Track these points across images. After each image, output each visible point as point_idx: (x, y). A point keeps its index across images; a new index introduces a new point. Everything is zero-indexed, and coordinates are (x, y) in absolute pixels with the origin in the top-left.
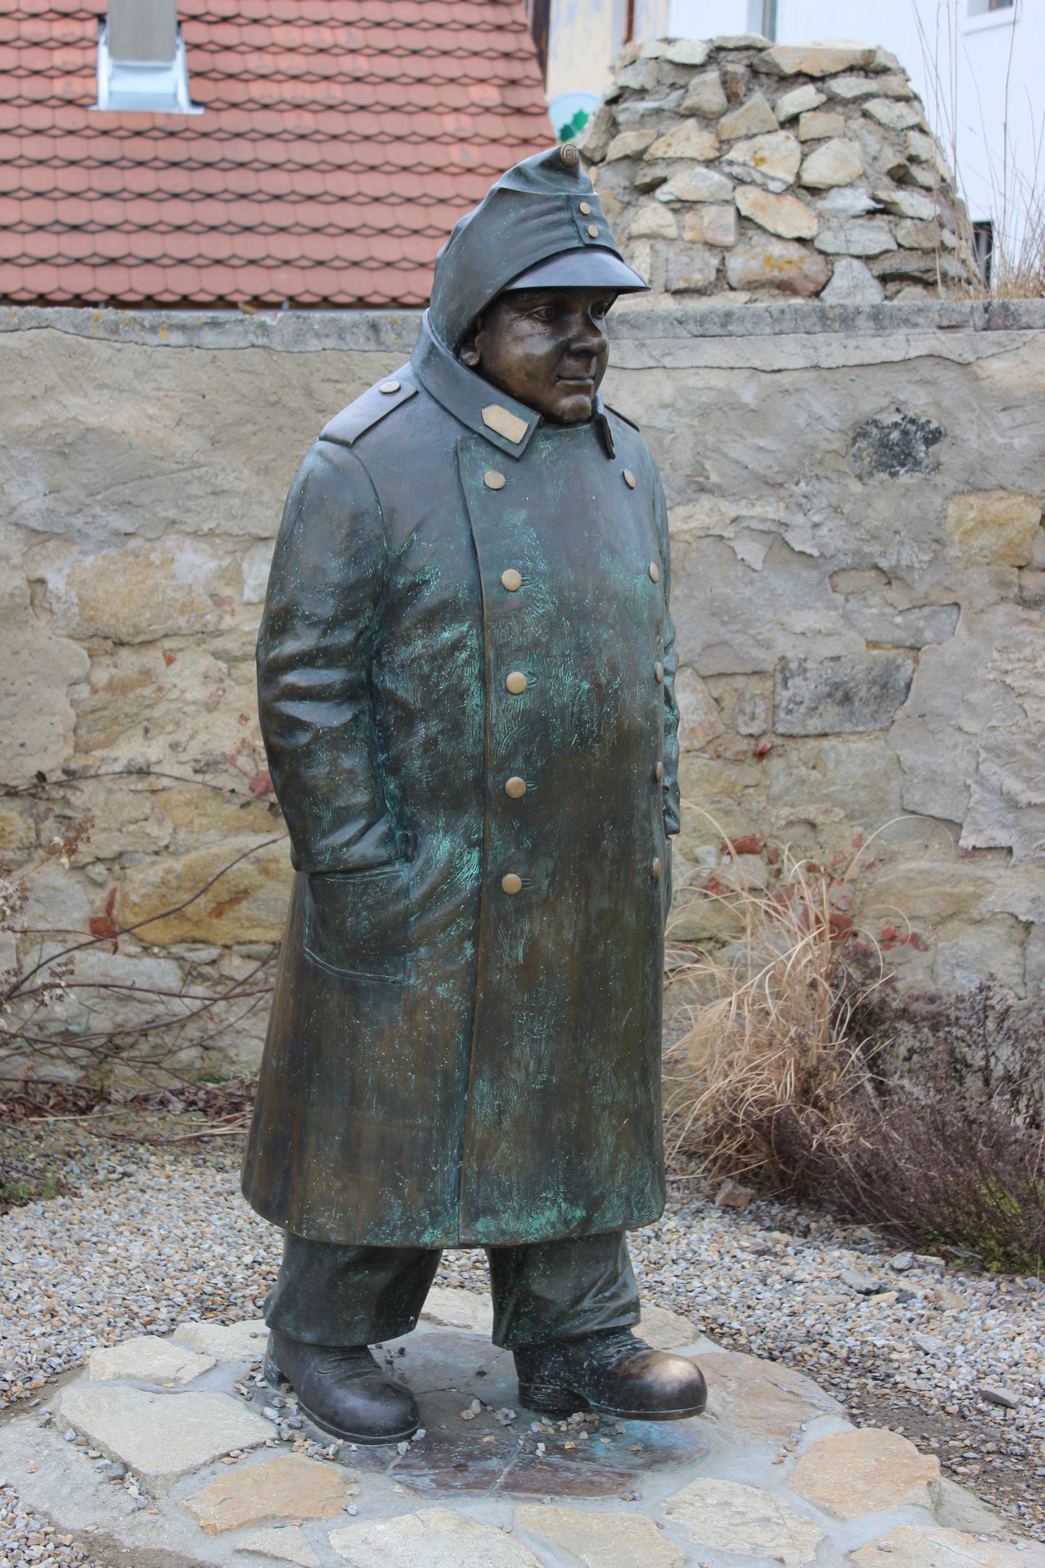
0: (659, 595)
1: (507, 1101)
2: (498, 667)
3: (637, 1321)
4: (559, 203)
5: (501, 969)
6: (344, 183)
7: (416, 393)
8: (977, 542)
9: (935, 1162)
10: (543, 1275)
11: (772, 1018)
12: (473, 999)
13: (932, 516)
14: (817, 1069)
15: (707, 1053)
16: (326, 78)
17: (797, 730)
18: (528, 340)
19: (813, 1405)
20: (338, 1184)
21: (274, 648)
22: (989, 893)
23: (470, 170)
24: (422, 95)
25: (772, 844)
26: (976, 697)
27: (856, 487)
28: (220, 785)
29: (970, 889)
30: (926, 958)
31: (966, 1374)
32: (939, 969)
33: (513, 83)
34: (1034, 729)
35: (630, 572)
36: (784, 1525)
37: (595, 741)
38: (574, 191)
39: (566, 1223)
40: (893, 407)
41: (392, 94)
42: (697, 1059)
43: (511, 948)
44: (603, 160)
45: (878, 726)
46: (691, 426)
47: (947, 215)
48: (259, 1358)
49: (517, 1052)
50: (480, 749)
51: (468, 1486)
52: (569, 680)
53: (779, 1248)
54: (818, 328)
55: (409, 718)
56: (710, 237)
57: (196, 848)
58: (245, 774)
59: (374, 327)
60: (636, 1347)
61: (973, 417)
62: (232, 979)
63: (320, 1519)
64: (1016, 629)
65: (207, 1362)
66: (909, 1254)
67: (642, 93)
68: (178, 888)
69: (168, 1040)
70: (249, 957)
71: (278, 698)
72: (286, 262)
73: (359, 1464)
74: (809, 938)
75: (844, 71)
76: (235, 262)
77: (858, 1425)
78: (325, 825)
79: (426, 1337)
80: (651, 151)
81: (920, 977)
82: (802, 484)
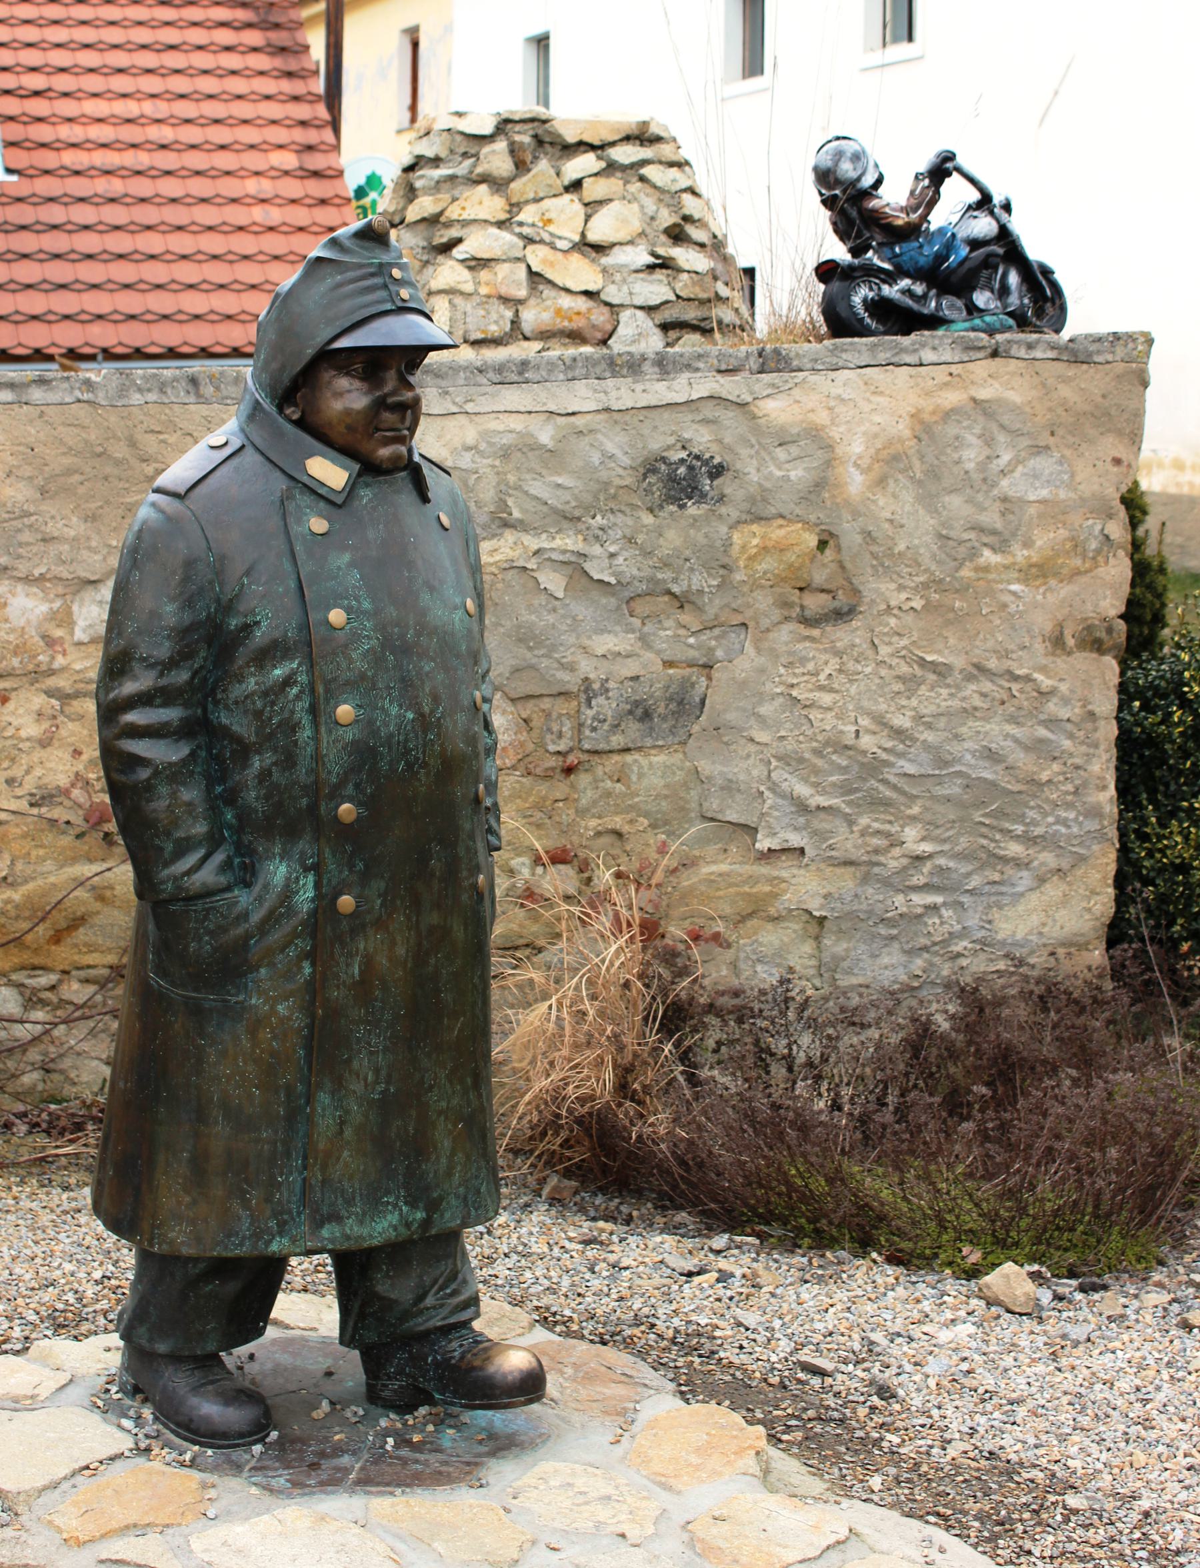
0: (476, 628)
1: (347, 1112)
2: (327, 701)
3: (477, 1315)
4: (372, 270)
5: (338, 987)
6: (153, 243)
7: (243, 447)
8: (761, 567)
9: (747, 1147)
10: (387, 1276)
11: (590, 1018)
12: (312, 1016)
13: (718, 543)
14: (632, 1065)
15: (530, 1055)
16: (134, 146)
17: (602, 746)
18: (347, 396)
19: (646, 1385)
20: (187, 1199)
21: (113, 689)
22: (785, 891)
23: (271, 229)
24: (224, 161)
25: (582, 854)
26: (765, 709)
27: (648, 519)
28: (56, 817)
29: (767, 889)
30: (729, 955)
31: (785, 1346)
32: (742, 965)
33: (310, 148)
34: (820, 738)
35: (448, 607)
36: (624, 1502)
37: (421, 767)
38: (385, 258)
39: (408, 1225)
40: (679, 445)
41: (196, 160)
42: (521, 1061)
43: (347, 965)
44: (402, 222)
45: (676, 740)
46: (493, 466)
47: (720, 268)
48: (113, 1371)
49: (355, 1064)
50: (312, 778)
51: (322, 1484)
52: (394, 710)
53: (604, 1236)
54: (608, 374)
55: (244, 751)
56: (503, 291)
57: (34, 879)
58: (80, 806)
59: (193, 381)
60: (478, 1340)
61: (753, 452)
62: (71, 1003)
63: (180, 1525)
64: (799, 646)
65: (63, 1378)
66: (727, 1236)
67: (436, 161)
68: (17, 918)
69: (11, 1064)
70: (87, 981)
71: (119, 737)
72: (100, 317)
73: (215, 1468)
74: (622, 942)
75: (621, 140)
76: (51, 317)
77: (687, 1401)
78: (167, 855)
79: (274, 1342)
80: (447, 213)
81: (724, 973)
82: (599, 517)
